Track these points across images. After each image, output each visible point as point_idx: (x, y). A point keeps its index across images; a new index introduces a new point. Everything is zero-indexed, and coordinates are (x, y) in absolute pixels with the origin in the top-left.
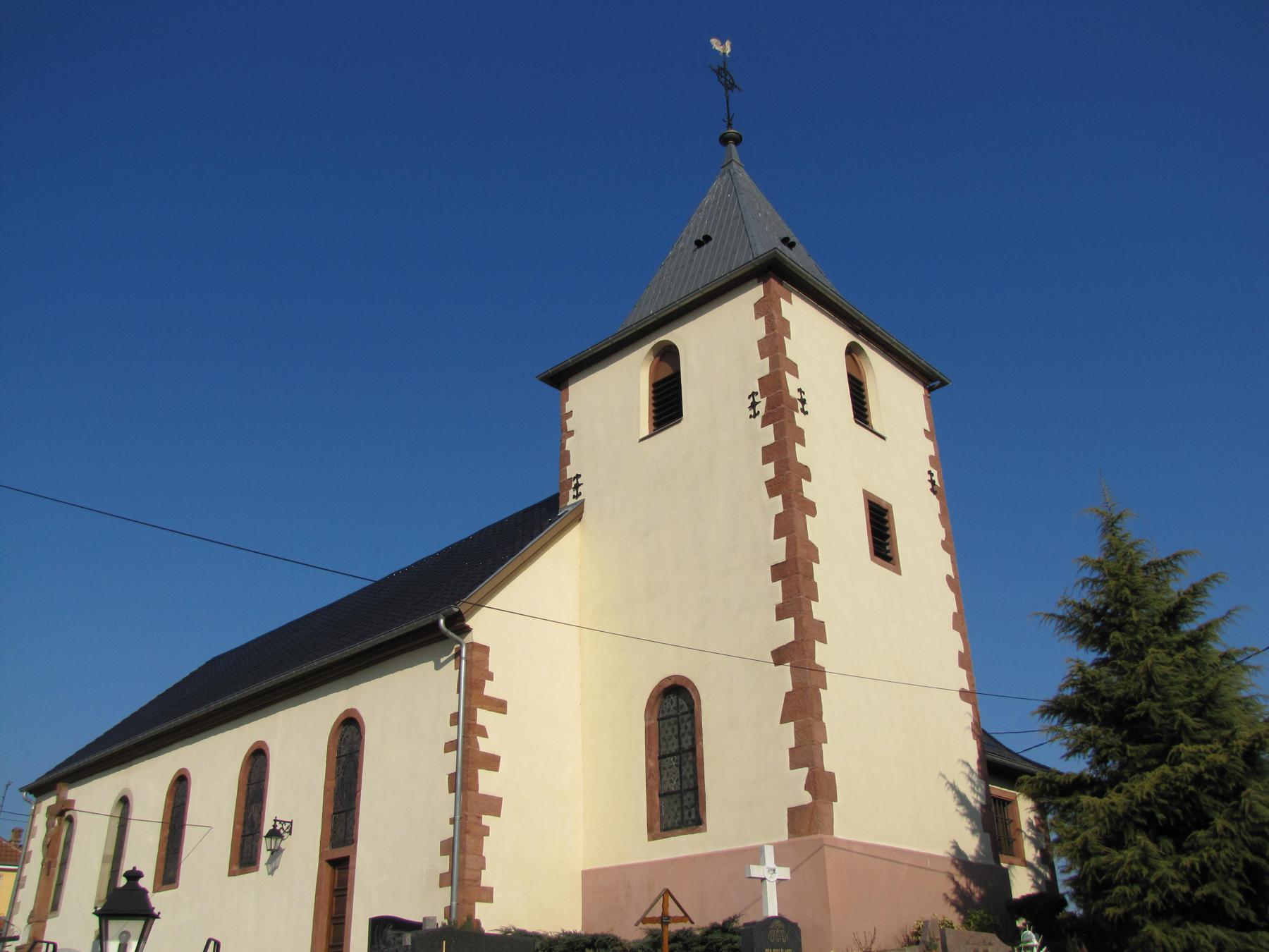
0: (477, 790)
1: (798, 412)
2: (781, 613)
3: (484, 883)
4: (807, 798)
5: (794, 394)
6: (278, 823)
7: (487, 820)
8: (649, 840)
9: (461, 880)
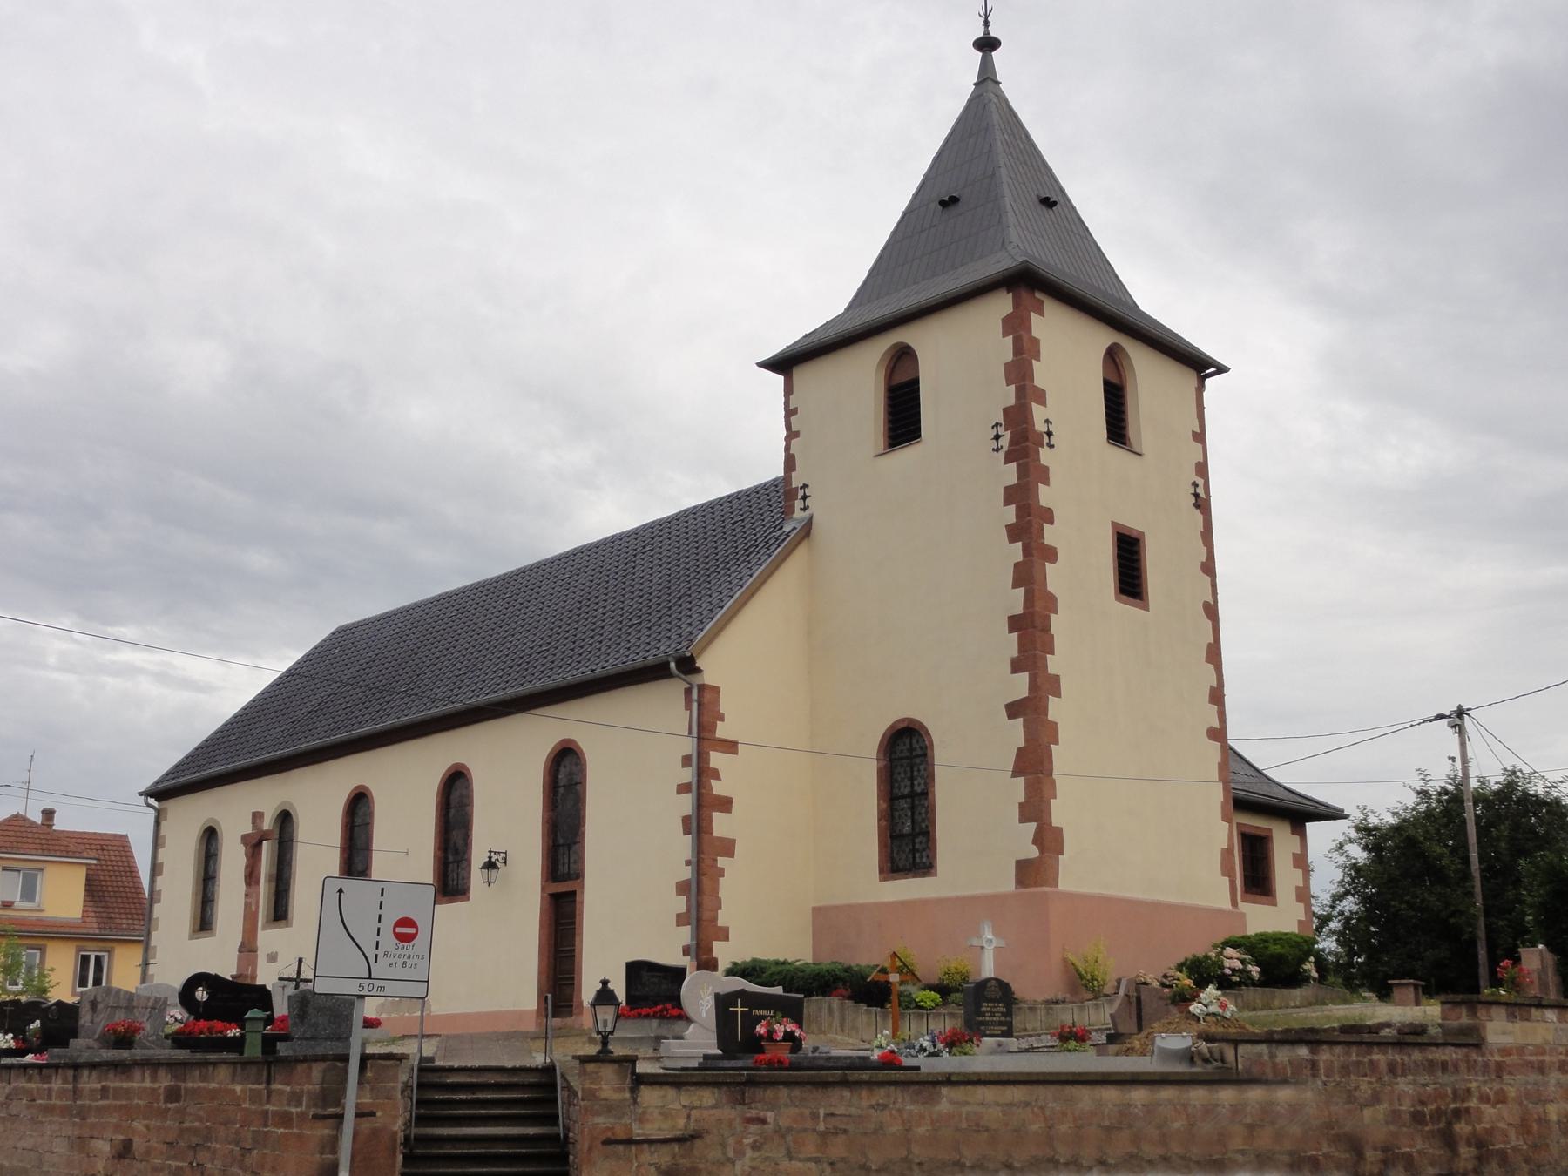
0: (712, 833)
1: (1043, 446)
2: (1017, 667)
3: (720, 923)
4: (1034, 852)
5: (1040, 427)
6: (492, 854)
7: (722, 862)
8: (880, 881)
9: (698, 920)
